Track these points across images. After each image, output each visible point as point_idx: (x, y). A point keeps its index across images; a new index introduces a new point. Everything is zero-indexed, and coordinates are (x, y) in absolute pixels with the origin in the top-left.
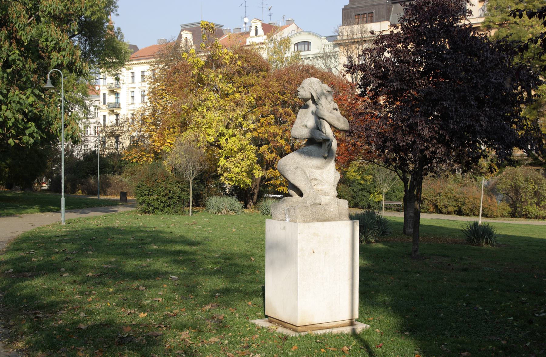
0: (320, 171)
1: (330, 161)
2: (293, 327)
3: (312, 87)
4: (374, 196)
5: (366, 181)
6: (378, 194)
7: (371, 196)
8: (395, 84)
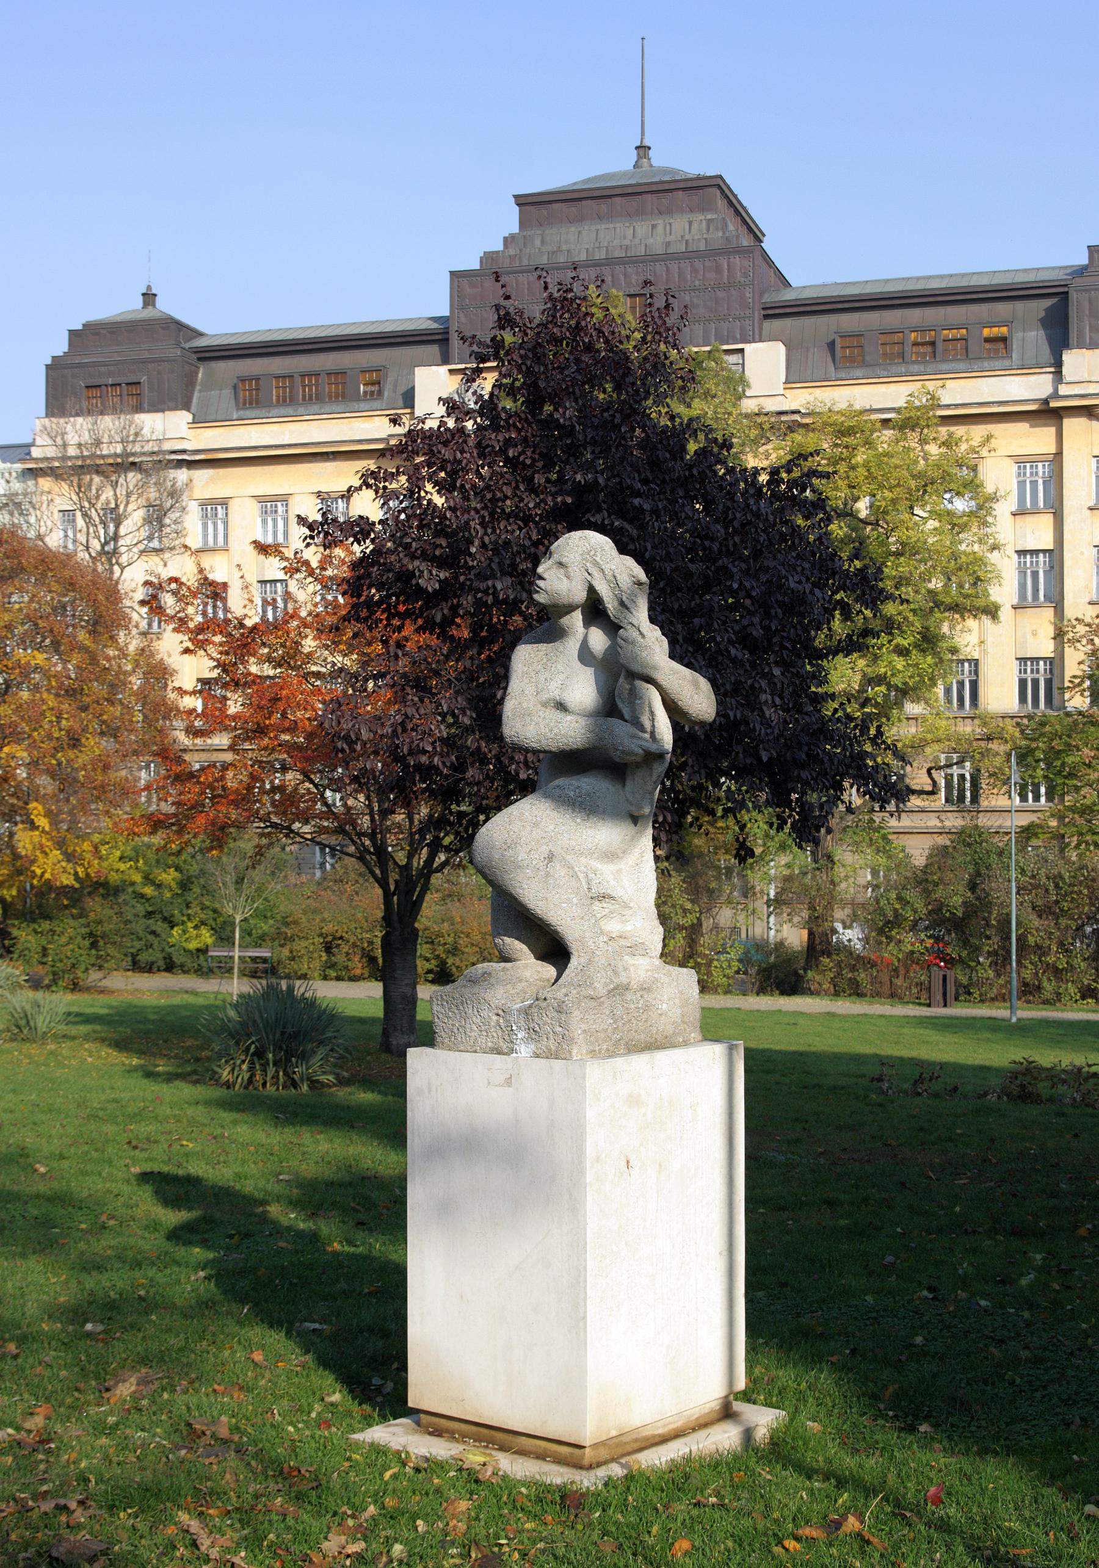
0: (611, 867)
1: (640, 833)
2: (566, 1452)
3: (596, 564)
4: (185, 932)
5: (159, 886)
6: (196, 927)
7: (176, 931)
8: (499, 586)
